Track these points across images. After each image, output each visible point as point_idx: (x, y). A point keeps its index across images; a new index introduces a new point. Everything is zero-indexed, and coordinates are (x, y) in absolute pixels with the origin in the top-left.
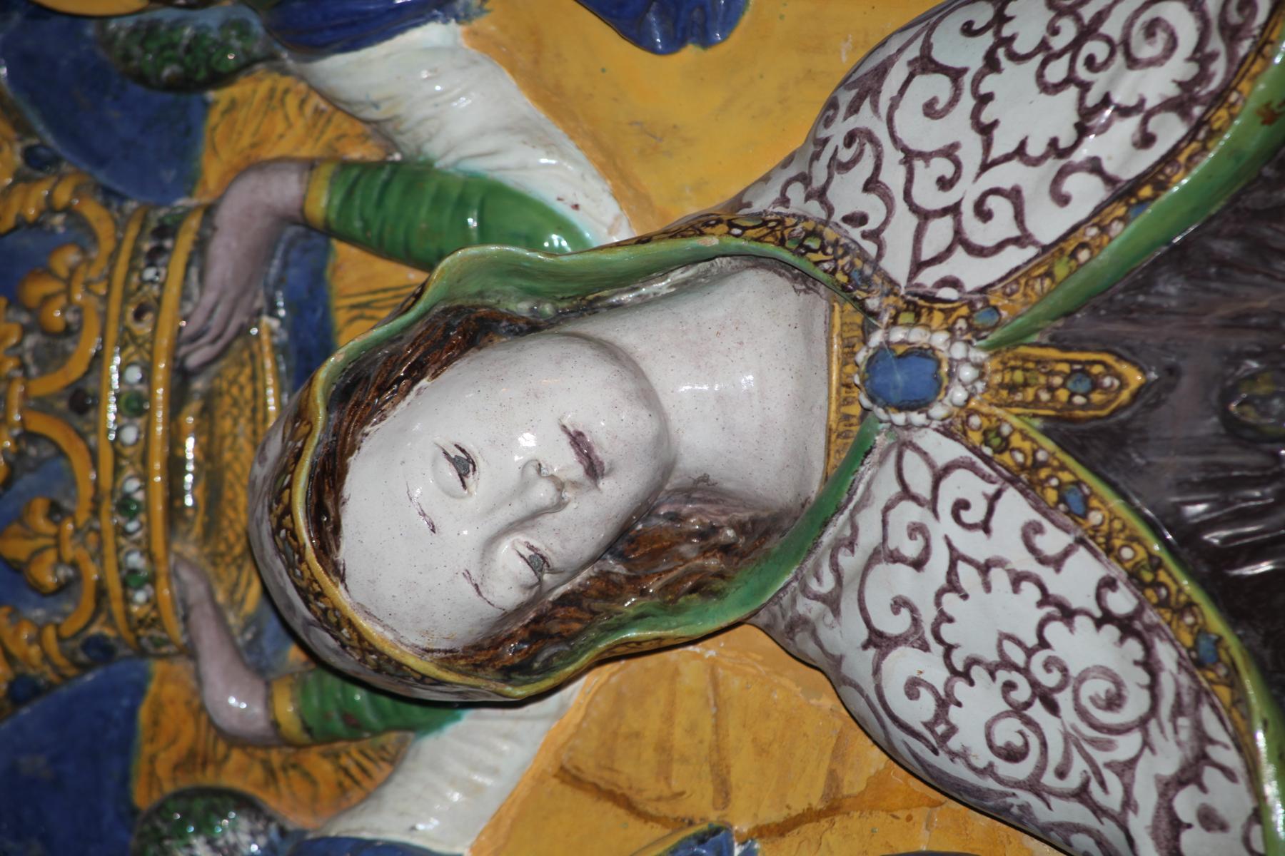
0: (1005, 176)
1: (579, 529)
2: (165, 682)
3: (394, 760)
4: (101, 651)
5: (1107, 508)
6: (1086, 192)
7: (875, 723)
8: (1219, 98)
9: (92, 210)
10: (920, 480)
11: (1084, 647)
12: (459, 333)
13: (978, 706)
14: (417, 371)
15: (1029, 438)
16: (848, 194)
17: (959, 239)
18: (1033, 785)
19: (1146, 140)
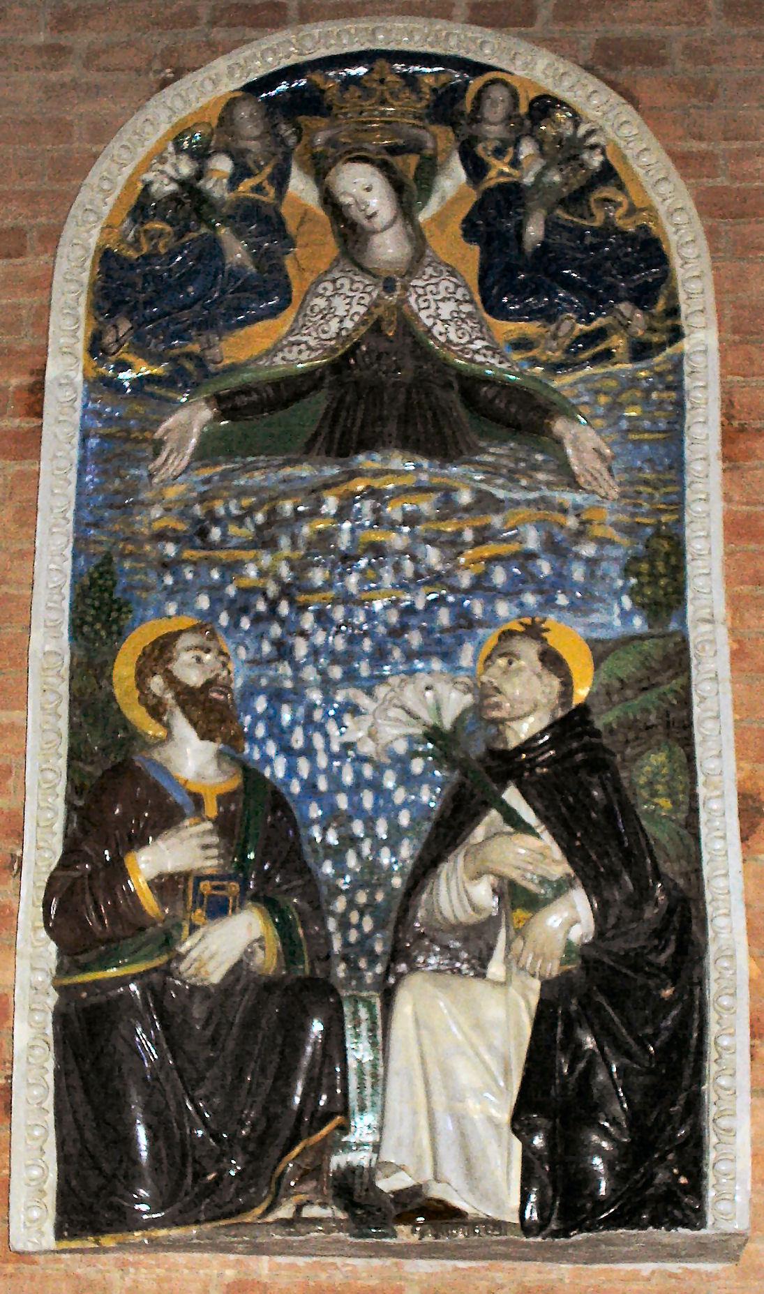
0: (433, 306)
1: (355, 213)
2: (322, 122)
3: (307, 173)
4: (330, 108)
5: (363, 330)
6: (429, 322)
7: (318, 282)
8: (449, 349)
9: (424, 103)
10: (369, 289)
11: (334, 325)
12: (398, 187)
13: (321, 303)
14: (389, 178)
15: (378, 312)
16: (429, 271)
17: (420, 296)
18: (305, 315)
19: (441, 334)
